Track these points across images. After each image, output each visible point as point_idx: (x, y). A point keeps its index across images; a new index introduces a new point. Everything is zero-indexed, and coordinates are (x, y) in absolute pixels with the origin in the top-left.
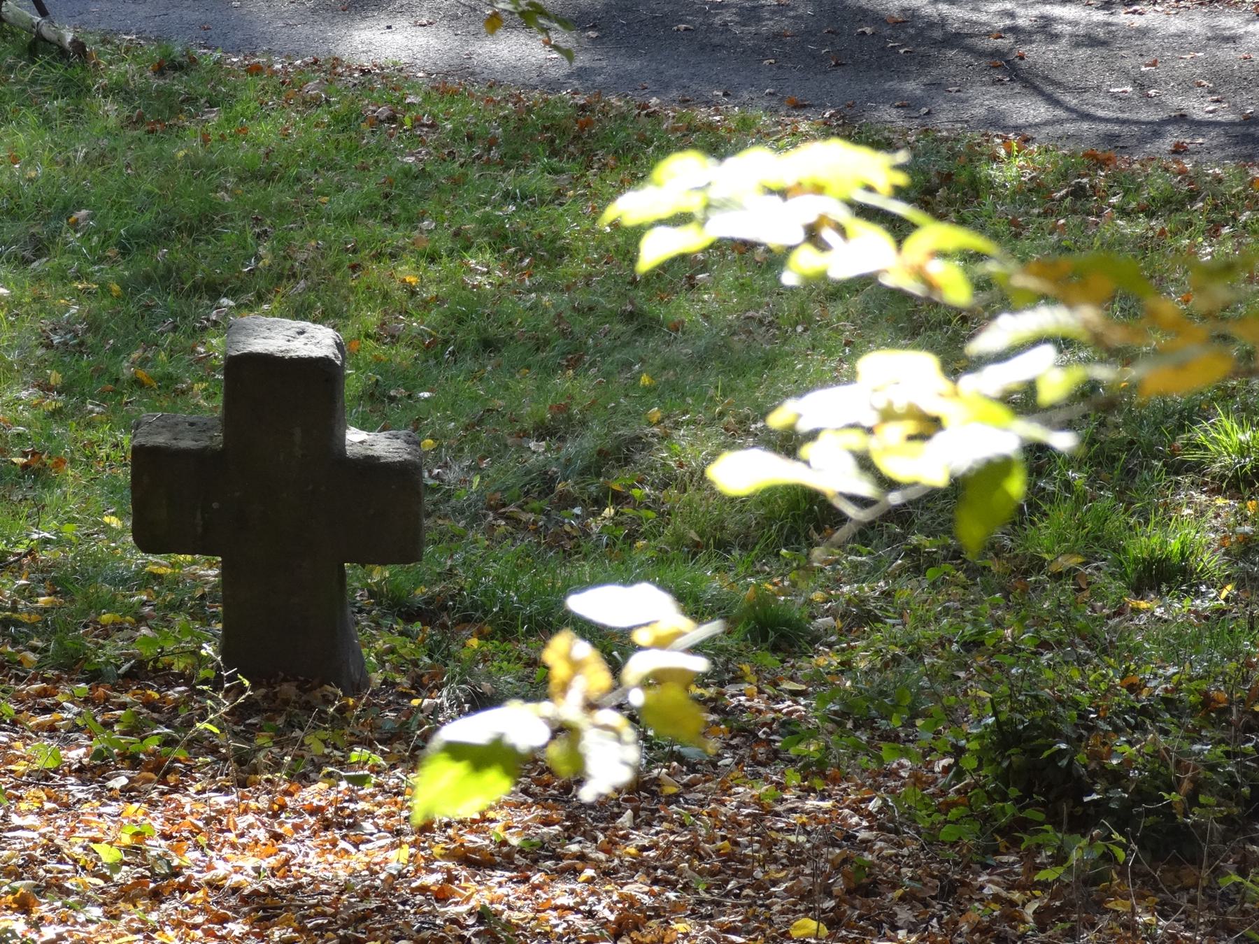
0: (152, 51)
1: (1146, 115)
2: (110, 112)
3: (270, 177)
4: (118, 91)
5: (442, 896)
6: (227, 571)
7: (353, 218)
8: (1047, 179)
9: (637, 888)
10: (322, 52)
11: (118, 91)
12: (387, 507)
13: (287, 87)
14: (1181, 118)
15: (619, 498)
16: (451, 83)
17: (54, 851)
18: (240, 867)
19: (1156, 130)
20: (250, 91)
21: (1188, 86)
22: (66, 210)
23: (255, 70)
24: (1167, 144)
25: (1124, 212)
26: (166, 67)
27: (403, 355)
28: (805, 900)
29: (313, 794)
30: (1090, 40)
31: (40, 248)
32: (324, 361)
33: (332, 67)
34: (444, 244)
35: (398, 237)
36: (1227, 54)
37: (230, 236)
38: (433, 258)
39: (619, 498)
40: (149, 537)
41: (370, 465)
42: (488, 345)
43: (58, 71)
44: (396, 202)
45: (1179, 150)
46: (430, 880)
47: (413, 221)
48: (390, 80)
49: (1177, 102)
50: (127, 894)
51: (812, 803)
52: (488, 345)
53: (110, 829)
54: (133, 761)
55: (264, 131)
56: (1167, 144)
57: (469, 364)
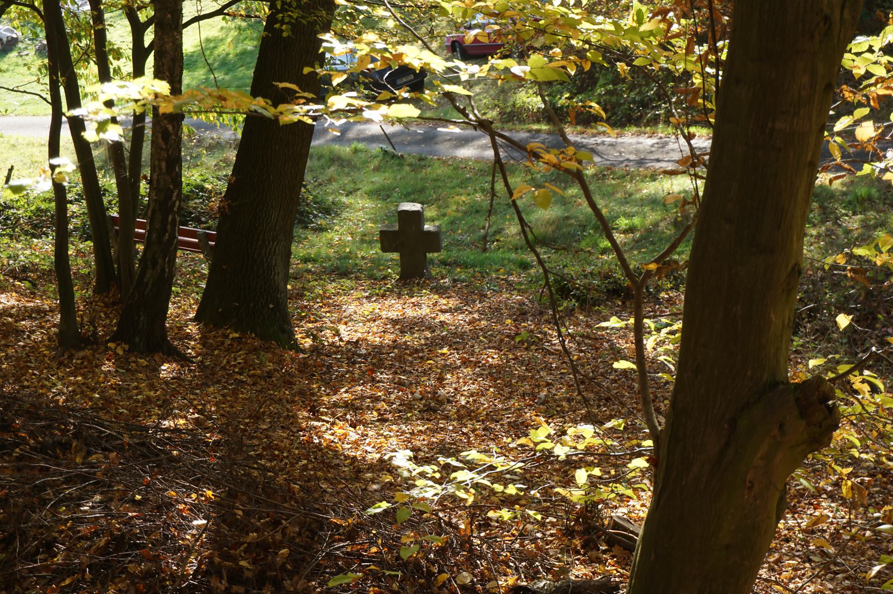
0: (418, 156)
1: (621, 159)
2: (407, 168)
3: (437, 180)
4: (410, 165)
5: (434, 318)
6: (401, 256)
7: (454, 188)
8: (670, 201)
9: (476, 316)
10: (454, 155)
11: (410, 165)
12: (433, 240)
13: (445, 162)
14: (628, 160)
15: (498, 241)
16: (478, 160)
17: (355, 313)
18: (393, 315)
19: (622, 162)
20: (437, 164)
21: (631, 153)
22: (394, 189)
23: (439, 159)
24: (624, 165)
25: (613, 179)
26: (421, 159)
27: (460, 215)
28: (510, 316)
29: (413, 300)
30: (611, 145)
31: (389, 197)
32: (418, 211)
33: (454, 158)
34: (472, 191)
35: (461, 191)
36: (640, 146)
37: (427, 192)
38: (469, 195)
39: (498, 241)
40: (384, 249)
41: (429, 232)
42: (477, 212)
43: (397, 161)
44: (463, 184)
45: (626, 166)
46: (433, 316)
47: (466, 188)
48: (466, 160)
49: (627, 156)
50: (369, 321)
51: (518, 297)
52: (477, 212)
53: (368, 308)
54: (377, 295)
55: (439, 172)
56: (624, 165)
57: (473, 215)
